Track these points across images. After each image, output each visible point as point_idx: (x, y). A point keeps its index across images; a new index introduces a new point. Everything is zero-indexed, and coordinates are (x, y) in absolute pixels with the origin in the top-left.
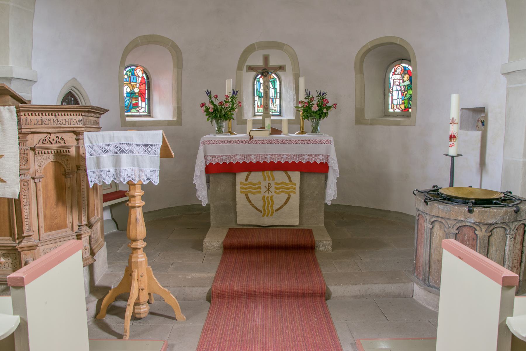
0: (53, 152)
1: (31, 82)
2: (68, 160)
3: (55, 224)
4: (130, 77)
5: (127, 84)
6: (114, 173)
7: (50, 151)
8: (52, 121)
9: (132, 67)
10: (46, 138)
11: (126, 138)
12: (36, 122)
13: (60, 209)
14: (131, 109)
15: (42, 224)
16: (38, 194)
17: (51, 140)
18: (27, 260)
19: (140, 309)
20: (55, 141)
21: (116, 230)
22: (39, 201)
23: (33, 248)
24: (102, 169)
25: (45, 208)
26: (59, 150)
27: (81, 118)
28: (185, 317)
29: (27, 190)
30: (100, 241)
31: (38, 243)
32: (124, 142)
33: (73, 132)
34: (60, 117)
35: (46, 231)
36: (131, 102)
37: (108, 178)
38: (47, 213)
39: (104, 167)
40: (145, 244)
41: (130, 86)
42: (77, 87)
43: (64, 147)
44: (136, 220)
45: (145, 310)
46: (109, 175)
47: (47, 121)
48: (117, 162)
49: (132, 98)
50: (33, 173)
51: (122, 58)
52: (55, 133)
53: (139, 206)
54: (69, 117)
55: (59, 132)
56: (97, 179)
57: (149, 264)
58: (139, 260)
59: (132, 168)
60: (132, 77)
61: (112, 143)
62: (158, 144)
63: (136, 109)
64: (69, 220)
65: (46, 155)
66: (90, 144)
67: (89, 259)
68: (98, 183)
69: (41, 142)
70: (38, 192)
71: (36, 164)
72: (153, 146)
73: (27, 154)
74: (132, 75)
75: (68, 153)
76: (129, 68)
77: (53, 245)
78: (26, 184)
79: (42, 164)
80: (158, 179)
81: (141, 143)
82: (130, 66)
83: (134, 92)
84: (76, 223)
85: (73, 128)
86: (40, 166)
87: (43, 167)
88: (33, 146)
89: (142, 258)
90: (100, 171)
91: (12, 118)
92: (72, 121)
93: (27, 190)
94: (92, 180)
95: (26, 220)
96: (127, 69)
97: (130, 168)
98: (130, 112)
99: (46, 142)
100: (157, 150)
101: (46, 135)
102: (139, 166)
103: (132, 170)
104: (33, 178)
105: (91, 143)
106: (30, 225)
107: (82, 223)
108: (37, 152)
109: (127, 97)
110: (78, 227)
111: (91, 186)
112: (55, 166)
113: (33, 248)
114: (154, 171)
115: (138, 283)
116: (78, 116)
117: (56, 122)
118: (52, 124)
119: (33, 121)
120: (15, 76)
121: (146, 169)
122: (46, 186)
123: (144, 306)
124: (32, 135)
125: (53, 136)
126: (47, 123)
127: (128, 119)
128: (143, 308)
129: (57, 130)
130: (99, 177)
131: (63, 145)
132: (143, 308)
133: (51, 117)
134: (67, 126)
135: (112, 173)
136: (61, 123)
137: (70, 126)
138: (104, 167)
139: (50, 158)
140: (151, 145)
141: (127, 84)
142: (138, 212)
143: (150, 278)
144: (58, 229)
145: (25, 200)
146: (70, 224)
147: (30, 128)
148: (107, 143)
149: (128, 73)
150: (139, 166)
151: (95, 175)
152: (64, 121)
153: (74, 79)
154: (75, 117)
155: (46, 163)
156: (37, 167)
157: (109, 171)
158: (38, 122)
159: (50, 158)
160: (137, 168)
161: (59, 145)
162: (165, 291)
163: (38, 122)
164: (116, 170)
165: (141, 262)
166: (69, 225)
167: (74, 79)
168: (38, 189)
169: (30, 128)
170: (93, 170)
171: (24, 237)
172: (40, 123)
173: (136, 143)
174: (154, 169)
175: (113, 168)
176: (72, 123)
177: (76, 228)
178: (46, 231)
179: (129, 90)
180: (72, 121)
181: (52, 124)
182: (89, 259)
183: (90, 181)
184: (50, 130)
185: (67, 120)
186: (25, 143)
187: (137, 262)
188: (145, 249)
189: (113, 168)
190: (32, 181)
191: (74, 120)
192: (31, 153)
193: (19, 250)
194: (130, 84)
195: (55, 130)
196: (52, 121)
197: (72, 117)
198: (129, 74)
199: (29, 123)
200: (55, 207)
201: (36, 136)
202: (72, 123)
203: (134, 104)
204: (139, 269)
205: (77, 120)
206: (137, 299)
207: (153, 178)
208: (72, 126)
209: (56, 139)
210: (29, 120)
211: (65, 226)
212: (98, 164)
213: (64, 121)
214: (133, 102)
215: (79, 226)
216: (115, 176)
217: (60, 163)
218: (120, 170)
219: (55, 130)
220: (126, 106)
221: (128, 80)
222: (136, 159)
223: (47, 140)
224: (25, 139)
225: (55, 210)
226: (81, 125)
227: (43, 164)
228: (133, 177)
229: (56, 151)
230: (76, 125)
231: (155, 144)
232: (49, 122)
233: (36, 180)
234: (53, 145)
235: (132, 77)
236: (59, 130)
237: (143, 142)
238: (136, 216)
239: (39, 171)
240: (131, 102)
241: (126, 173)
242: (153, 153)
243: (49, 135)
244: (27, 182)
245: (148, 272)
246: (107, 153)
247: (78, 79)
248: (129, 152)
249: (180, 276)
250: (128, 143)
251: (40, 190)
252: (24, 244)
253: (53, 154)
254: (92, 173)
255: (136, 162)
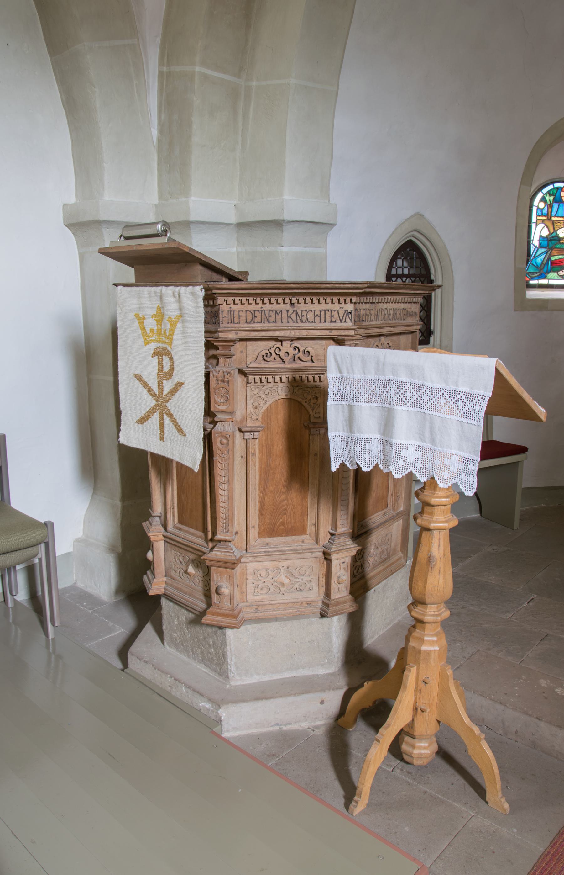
0: (284, 379)
1: (323, 226)
2: (317, 398)
3: (283, 524)
4: (550, 206)
5: (543, 221)
6: (380, 447)
7: (277, 378)
8: (285, 315)
9: (556, 185)
10: (272, 351)
11: (410, 370)
12: (249, 318)
13: (294, 496)
14: (548, 272)
15: (254, 520)
16: (251, 463)
17: (282, 353)
18: (220, 584)
19: (413, 747)
20: (291, 355)
21: (477, 515)
22: (251, 477)
23: (230, 565)
24: (357, 435)
25: (263, 490)
26: (297, 377)
27: (350, 307)
28: (506, 806)
29: (226, 452)
30: (395, 558)
31: (241, 557)
32: (404, 380)
33: (333, 339)
34: (303, 306)
35: (261, 534)
36: (549, 258)
37: (367, 456)
38: (266, 500)
39: (360, 432)
40: (446, 614)
41: (550, 224)
42: (424, 231)
43: (307, 370)
44: (430, 559)
45: (423, 752)
46: (370, 452)
47: (273, 315)
48: (387, 424)
49: (552, 249)
50: (242, 421)
51: (527, 167)
52: (292, 340)
53: (440, 529)
54: (323, 306)
55: (299, 339)
56: (347, 455)
57: (449, 661)
58: (424, 648)
59: (417, 443)
60: (555, 206)
61: (381, 377)
62: (481, 392)
63: (557, 271)
64: (311, 520)
65: (270, 385)
66: (338, 375)
67: (344, 602)
68: (348, 465)
69: (260, 358)
70: (251, 458)
71: (250, 402)
72: (470, 397)
73: (228, 382)
74: (555, 201)
75: (318, 383)
76: (550, 187)
77: (274, 563)
78: (225, 441)
79: (262, 403)
80: (474, 481)
81: (443, 386)
82: (553, 183)
83: (557, 236)
84: (326, 527)
85: (331, 330)
86: (256, 408)
87: (265, 408)
88: (242, 366)
89: (432, 643)
90: (350, 439)
91: (196, 311)
92: (328, 314)
93: (226, 452)
94: (337, 455)
95: (221, 509)
96: (545, 190)
97: (413, 442)
98: (545, 278)
99: (271, 359)
100: (477, 408)
101: (272, 343)
102: (433, 442)
103: (418, 448)
104: (240, 431)
105: (341, 372)
106: (230, 520)
107: (336, 530)
108: (251, 378)
109: (541, 246)
110: (329, 536)
111: (334, 469)
112: (290, 407)
113: (230, 565)
114: (467, 461)
115: (416, 695)
116: (343, 305)
117: (294, 316)
118: (285, 320)
119: (243, 314)
120: (192, 219)
121: (449, 451)
122: (266, 449)
123: (424, 744)
124: (244, 343)
125: (287, 346)
126: (272, 319)
127: (532, 294)
128: (420, 748)
129: (293, 333)
130: (350, 451)
131: (308, 365)
132: (420, 748)
133: (282, 306)
134: (317, 325)
135: (375, 447)
136: (304, 319)
137: (323, 325)
138: (360, 432)
139: (279, 391)
140: (467, 394)
141: (543, 221)
142: (435, 542)
143: (444, 691)
144: (287, 535)
145: (222, 473)
146: (314, 529)
147: (236, 331)
148: (370, 378)
149: (547, 198)
150: (433, 442)
151: (343, 445)
152: (310, 316)
153: (419, 215)
154: (336, 306)
155: (270, 401)
156: (250, 409)
157: (369, 441)
158: (254, 317)
159: (279, 391)
160: (429, 445)
161: (298, 365)
162: (472, 731)
163: (254, 317)
164: (384, 442)
165: (428, 653)
166: (310, 528)
167: (419, 215)
168: (251, 451)
169: (236, 331)
170: (341, 433)
171: (220, 541)
172: (258, 319)
173: (430, 385)
174: (467, 455)
175: (379, 436)
176: (328, 319)
177: (324, 538)
178: (261, 534)
179: (545, 233)
180: (328, 314)
181: (285, 320)
182: (344, 602)
183: (332, 455)
184: (277, 334)
185: (317, 313)
186: (227, 360)
187: (419, 651)
188: (444, 624)
189: (379, 436)
190: (238, 434)
191: (335, 314)
192: (239, 380)
193: (208, 563)
194: (549, 219)
195: (288, 333)
196: (285, 315)
197: (330, 306)
198: (549, 198)
199: (236, 320)
200: (284, 490)
201: (251, 345)
202: (328, 319)
203: (553, 263)
204: (422, 666)
205: (342, 313)
206: (408, 725)
207: (463, 477)
208: (328, 324)
209: (292, 352)
210: (236, 314)
211: (302, 531)
212: (350, 422)
213: (310, 316)
214: (553, 258)
215: (332, 535)
216: (382, 456)
217: (300, 403)
218: (391, 445)
219: (288, 333)
220: (537, 267)
221: (545, 211)
222: (427, 424)
223: (273, 354)
224: (227, 352)
225: (283, 497)
226: (349, 323)
227: (259, 403)
228: (419, 465)
229: (290, 377)
230: (338, 324)
231: (476, 392)
232: (279, 317)
233: (247, 435)
234: (286, 365)
235: (555, 206)
236: (297, 333)
237: (446, 383)
238: (429, 551)
239: (254, 417)
240: (549, 258)
241: (403, 453)
242: (468, 415)
243: (278, 345)
244: (226, 438)
245: (443, 677)
246: (370, 400)
247: (428, 215)
248: (414, 405)
249: (543, 683)
250: (413, 381)
251: (254, 454)
252: (217, 554)
253: (286, 384)
254: (338, 439)
255: (428, 431)
